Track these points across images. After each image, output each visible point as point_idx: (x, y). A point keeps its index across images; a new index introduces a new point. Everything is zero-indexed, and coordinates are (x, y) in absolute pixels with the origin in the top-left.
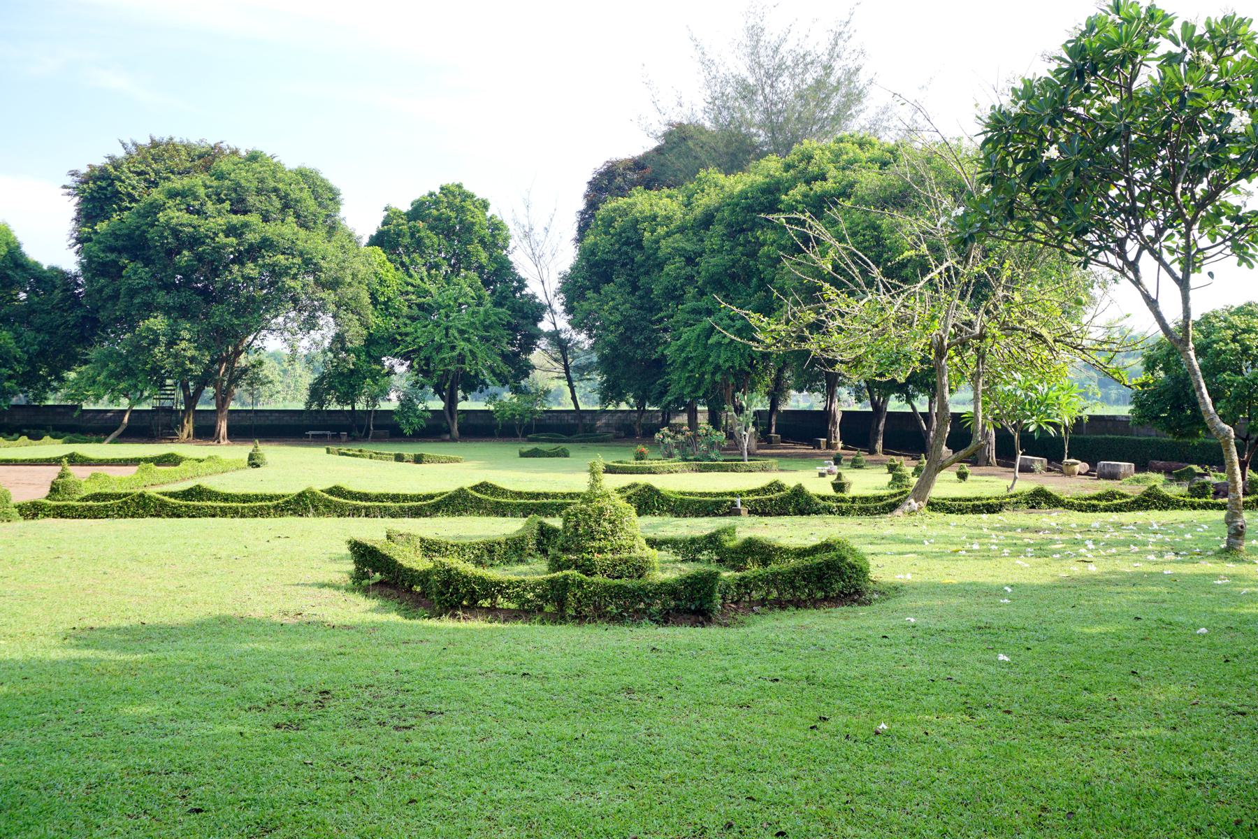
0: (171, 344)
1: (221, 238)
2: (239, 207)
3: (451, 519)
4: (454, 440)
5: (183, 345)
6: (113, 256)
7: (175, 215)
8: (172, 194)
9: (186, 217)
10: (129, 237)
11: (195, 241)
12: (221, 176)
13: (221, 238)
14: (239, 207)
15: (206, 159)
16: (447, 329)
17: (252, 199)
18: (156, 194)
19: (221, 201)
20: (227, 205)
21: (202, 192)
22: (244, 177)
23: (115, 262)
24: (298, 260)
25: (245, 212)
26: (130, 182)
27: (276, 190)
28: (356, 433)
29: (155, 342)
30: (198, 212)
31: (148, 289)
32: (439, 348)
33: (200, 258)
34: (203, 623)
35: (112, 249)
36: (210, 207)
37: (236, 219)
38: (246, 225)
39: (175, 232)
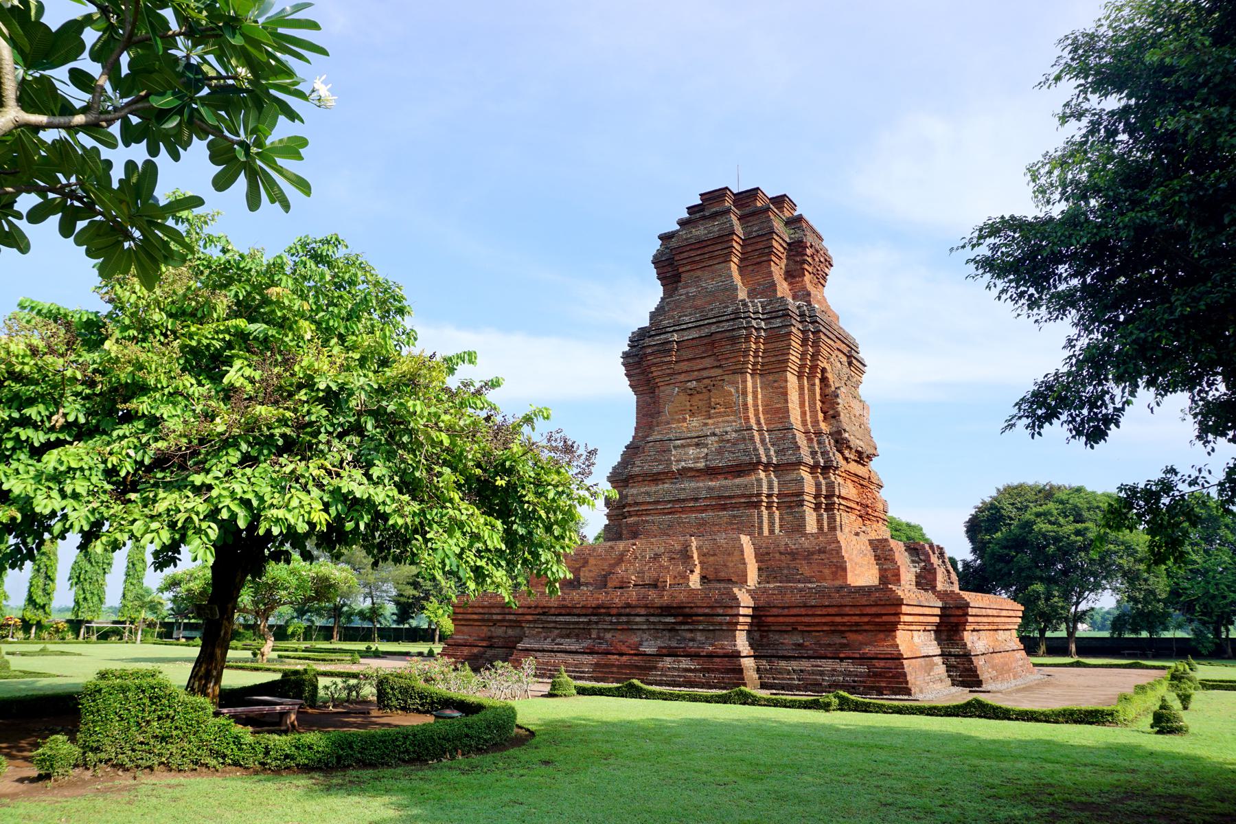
0: (1047, 599)
1: (1073, 537)
2: (1079, 519)
3: (1065, 707)
4: (1229, 658)
5: (1056, 599)
6: (1006, 551)
7: (1042, 526)
8: (1038, 515)
9: (1050, 527)
10: (1015, 540)
11: (1057, 539)
12: (1062, 502)
13: (1073, 537)
14: (1079, 519)
15: (1047, 493)
16: (1216, 584)
17: (1086, 514)
18: (1028, 516)
19: (1066, 516)
20: (1071, 518)
21: (1055, 512)
22: (1075, 500)
23: (1008, 555)
24: (1122, 547)
25: (1083, 522)
26: (1009, 511)
27: (1098, 507)
28: (757, 635)
29: (1038, 598)
30: (1054, 524)
31: (1030, 568)
32: (1213, 597)
33: (1059, 549)
34: (411, 762)
35: (1005, 547)
36: (1061, 520)
37: (1079, 526)
38: (1086, 529)
39: (1044, 536)
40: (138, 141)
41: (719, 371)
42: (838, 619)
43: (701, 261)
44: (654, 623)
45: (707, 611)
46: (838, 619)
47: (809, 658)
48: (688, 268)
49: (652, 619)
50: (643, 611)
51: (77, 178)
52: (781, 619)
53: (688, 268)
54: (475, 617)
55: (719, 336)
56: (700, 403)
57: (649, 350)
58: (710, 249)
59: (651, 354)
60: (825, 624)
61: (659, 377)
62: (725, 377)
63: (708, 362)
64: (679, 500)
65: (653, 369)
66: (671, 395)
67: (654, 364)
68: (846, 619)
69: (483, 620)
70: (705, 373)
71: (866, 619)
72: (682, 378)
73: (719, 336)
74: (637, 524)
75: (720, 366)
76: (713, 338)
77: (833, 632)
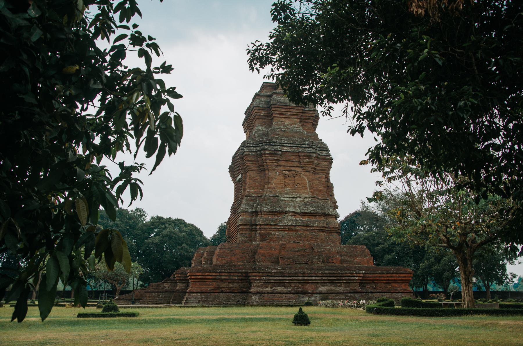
40: (133, 15)
41: (300, 169)
42: (390, 279)
43: (285, 114)
44: (325, 280)
45: (349, 275)
46: (390, 279)
47: (380, 293)
48: (278, 116)
49: (324, 278)
50: (301, 275)
51: (494, 178)
52: (369, 278)
53: (278, 116)
54: (210, 277)
55: (303, 154)
56: (289, 182)
57: (267, 152)
58: (291, 110)
59: (268, 154)
60: (385, 280)
61: (270, 165)
62: (303, 172)
63: (295, 164)
64: (287, 225)
65: (268, 161)
66: (276, 176)
67: (269, 159)
68: (393, 278)
69: (215, 279)
70: (293, 169)
71: (400, 278)
72: (281, 168)
73: (303, 154)
74: (266, 234)
75: (301, 167)
76: (300, 154)
77: (387, 283)
